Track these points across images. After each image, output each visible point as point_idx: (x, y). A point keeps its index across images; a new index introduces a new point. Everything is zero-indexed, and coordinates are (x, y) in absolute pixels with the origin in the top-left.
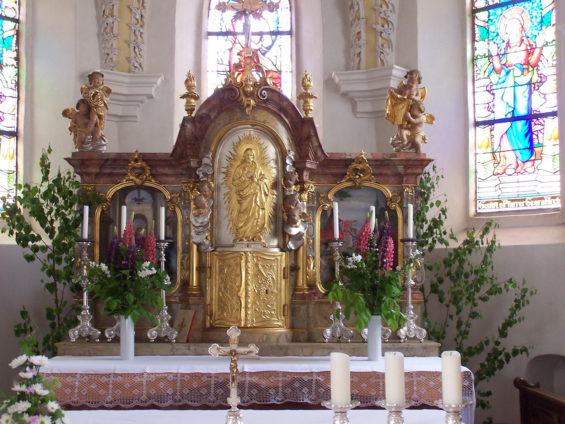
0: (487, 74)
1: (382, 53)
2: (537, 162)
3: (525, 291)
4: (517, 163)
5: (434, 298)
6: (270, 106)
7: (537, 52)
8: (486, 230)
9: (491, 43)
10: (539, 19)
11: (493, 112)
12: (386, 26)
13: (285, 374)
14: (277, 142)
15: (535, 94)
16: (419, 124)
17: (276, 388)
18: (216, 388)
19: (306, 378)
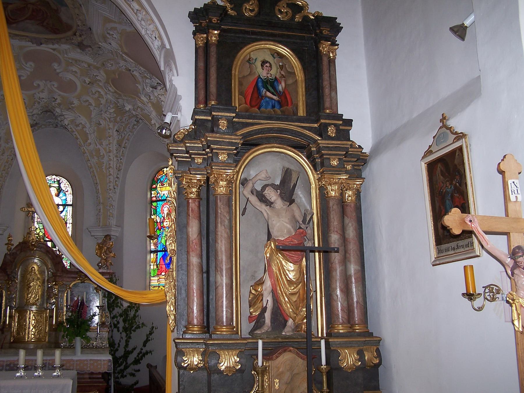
1: (109, 219)
4: (166, 270)
5: (115, 330)
6: (42, 250)
9: (158, 217)
12: (111, 207)
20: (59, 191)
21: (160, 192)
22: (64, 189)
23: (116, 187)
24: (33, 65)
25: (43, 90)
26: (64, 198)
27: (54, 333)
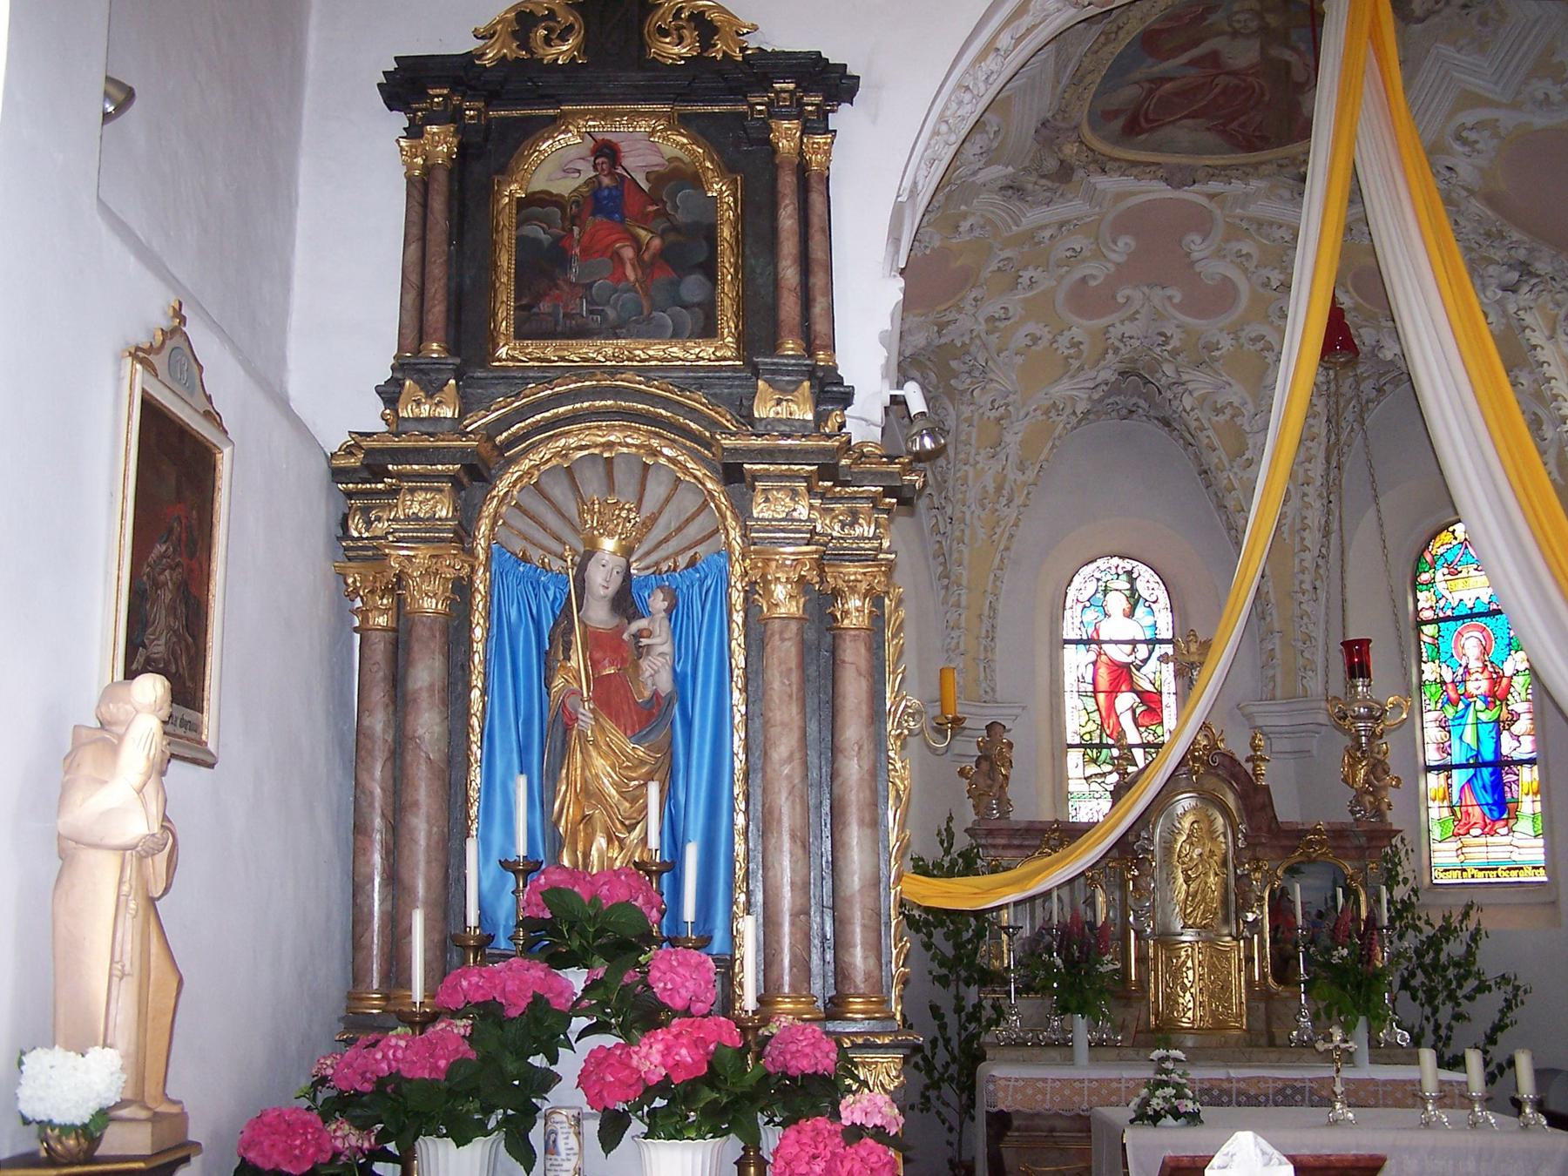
0: (1439, 705)
2: (1511, 822)
3: (1517, 988)
7: (1505, 681)
8: (1466, 915)
9: (1444, 666)
10: (1507, 641)
11: (1449, 754)
13: (1276, 1080)
14: (1225, 811)
15: (1505, 736)
16: (1385, 788)
17: (1267, 1096)
18: (1237, 1096)
19: (1298, 1085)
20: (1132, 600)
21: (1446, 593)
22: (1145, 593)
23: (1318, 584)
24: (1133, 244)
25: (1137, 312)
26: (1149, 620)
27: (1262, 1006)
